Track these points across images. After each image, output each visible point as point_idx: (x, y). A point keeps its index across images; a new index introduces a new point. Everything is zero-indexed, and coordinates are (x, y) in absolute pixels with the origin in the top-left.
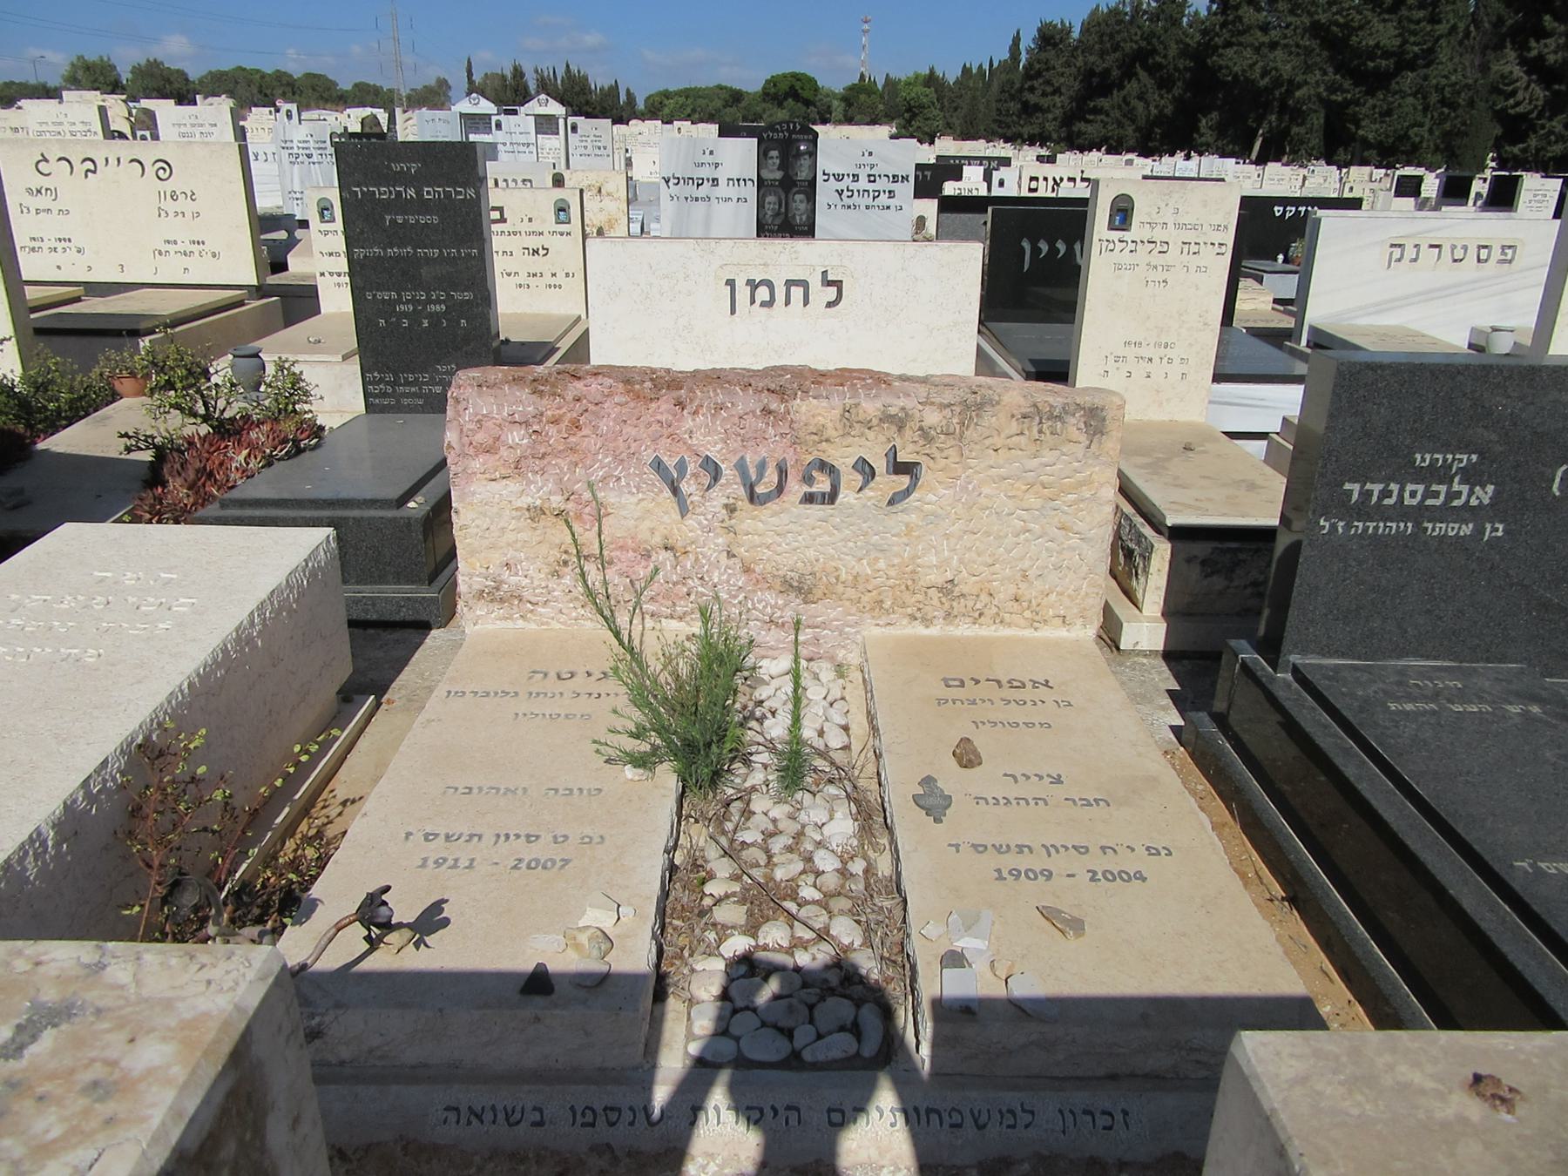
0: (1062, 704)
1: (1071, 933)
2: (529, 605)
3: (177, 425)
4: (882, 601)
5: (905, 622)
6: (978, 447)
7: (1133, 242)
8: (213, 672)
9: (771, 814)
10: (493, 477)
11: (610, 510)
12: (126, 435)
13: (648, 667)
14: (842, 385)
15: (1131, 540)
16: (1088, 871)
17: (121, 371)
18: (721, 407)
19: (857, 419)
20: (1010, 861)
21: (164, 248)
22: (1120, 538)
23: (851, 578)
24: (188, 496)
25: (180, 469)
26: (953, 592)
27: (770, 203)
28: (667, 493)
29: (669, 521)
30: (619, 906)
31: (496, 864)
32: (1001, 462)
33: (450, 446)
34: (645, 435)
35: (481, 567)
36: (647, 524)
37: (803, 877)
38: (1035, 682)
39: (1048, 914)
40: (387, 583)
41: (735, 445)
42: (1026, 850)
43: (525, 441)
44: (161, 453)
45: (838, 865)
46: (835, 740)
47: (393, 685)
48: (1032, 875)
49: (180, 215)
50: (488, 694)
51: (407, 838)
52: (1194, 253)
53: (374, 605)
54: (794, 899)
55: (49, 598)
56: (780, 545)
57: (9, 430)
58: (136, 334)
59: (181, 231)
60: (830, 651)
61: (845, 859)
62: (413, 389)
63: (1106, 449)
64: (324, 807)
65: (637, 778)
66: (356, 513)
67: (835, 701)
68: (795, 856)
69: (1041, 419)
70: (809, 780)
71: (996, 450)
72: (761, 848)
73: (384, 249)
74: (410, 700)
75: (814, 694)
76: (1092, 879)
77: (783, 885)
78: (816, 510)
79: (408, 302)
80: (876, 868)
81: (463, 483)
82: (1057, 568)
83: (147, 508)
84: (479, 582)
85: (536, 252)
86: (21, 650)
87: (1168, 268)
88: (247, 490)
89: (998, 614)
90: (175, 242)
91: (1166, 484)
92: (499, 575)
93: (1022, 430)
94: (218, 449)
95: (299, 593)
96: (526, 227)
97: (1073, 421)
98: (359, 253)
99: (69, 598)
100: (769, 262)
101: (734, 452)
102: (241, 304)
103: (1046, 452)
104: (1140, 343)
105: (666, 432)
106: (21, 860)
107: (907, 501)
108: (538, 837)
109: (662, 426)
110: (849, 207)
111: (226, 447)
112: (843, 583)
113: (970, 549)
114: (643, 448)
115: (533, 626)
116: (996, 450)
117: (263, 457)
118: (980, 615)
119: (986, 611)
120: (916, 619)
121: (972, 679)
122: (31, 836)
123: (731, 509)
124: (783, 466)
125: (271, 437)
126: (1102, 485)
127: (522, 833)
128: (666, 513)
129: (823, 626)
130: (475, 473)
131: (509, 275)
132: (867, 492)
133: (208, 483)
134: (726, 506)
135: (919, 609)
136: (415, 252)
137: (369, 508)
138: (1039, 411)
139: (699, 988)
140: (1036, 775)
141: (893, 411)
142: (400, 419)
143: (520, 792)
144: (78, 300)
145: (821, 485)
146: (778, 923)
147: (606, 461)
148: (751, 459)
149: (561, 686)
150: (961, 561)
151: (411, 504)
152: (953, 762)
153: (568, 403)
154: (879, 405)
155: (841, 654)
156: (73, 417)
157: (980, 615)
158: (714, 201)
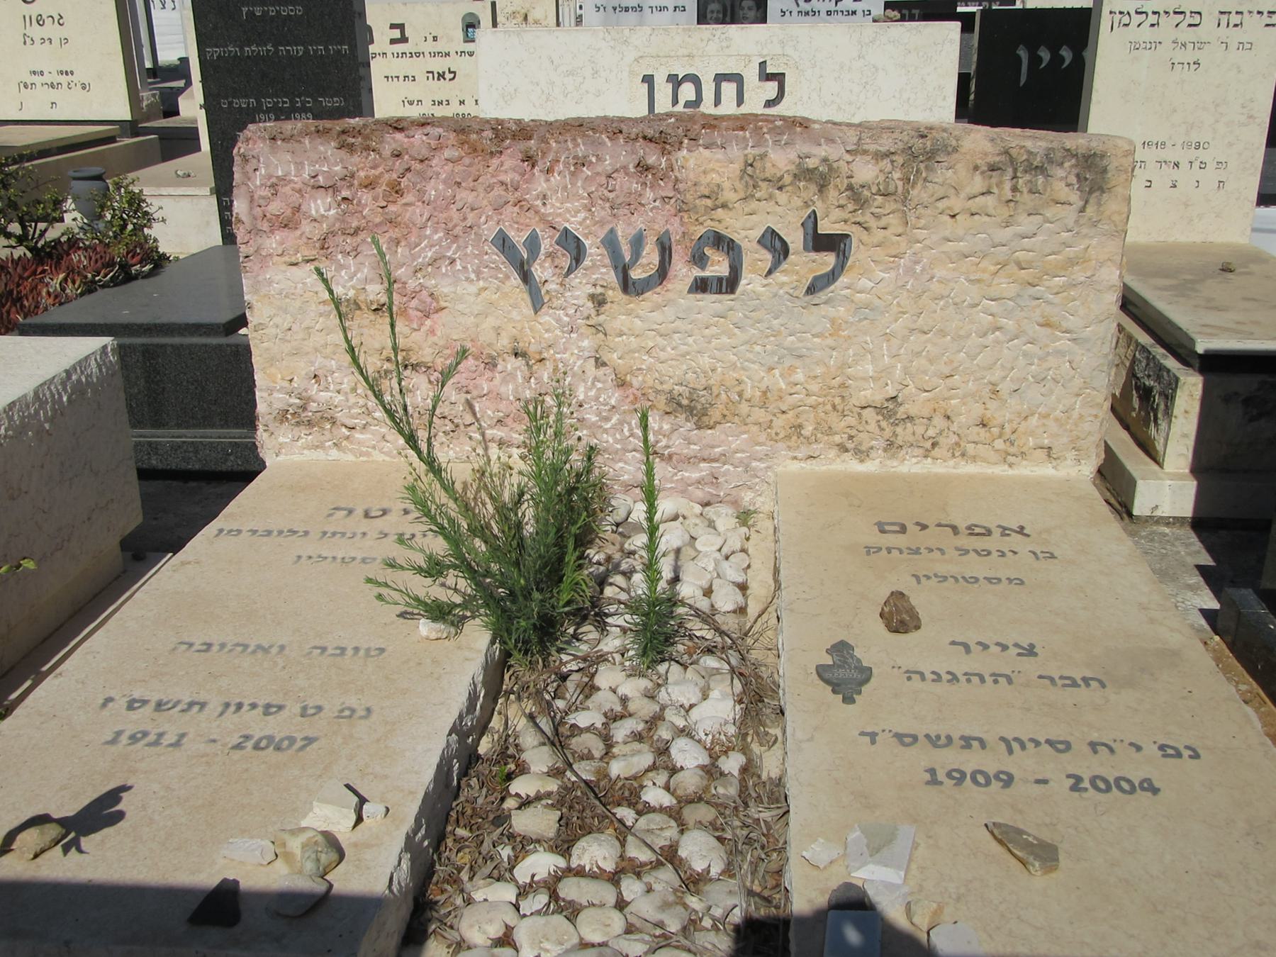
0: (1041, 555)
1: (1037, 864)
2: (344, 430)
4: (800, 426)
5: (832, 453)
6: (929, 211)
7: (1154, 13)
9: (621, 691)
10: (293, 260)
11: (443, 304)
13: (453, 483)
14: (742, 129)
15: (1149, 376)
16: (1069, 776)
18: (581, 163)
19: (762, 176)
20: (950, 758)
21: (30, 79)
22: (1134, 375)
23: (758, 394)
26: (895, 413)
27: (712, 12)
28: (515, 280)
29: (519, 318)
30: (363, 801)
31: (214, 741)
32: (961, 232)
33: (239, 221)
34: (485, 202)
35: (283, 379)
36: (490, 322)
37: (650, 774)
38: (1005, 529)
39: (1004, 836)
40: (213, 426)
41: (603, 213)
42: (975, 744)
43: (333, 212)
45: (704, 759)
46: (726, 600)
48: (981, 778)
49: (47, 42)
50: (269, 533)
51: (104, 705)
52: (1236, 25)
53: (196, 452)
54: (631, 805)
56: (663, 350)
59: (47, 60)
60: (734, 492)
61: (715, 752)
63: (1107, 213)
65: (433, 636)
66: (177, 340)
67: (733, 553)
68: (644, 747)
69: (1015, 170)
70: (680, 648)
71: (953, 216)
72: (600, 735)
73: (242, 49)
75: (704, 545)
76: (1075, 788)
77: (620, 784)
78: (710, 302)
80: (760, 768)
82: (1040, 380)
85: (441, 76)
87: (1199, 45)
89: (957, 444)
90: (42, 73)
91: (1196, 306)
92: (306, 390)
93: (990, 187)
94: (34, 273)
95: (53, 409)
96: (429, 47)
97: (1060, 173)
98: (214, 52)
100: (695, 52)
101: (602, 223)
102: (111, 139)
103: (1023, 218)
104: (1163, 144)
105: (511, 197)
107: (832, 287)
108: (280, 708)
109: (507, 190)
110: (807, 13)
112: (749, 401)
113: (918, 354)
114: (483, 219)
115: (350, 457)
116: (953, 216)
118: (934, 445)
119: (941, 440)
120: (847, 451)
121: (918, 524)
123: (599, 301)
124: (665, 240)
126: (1102, 264)
127: (261, 702)
128: (515, 306)
129: (723, 458)
131: (411, 103)
132: (779, 277)
133: (13, 309)
134: (592, 297)
135: (851, 437)
136: (277, 51)
137: (192, 334)
138: (1012, 160)
139: (471, 926)
140: (998, 644)
141: (811, 163)
143: (274, 650)
145: (717, 268)
146: (603, 837)
147: (436, 237)
148: (624, 233)
149: (365, 525)
150: (906, 371)
152: (880, 626)
153: (385, 160)
154: (793, 155)
155: (747, 497)
157: (934, 445)
158: (647, 11)
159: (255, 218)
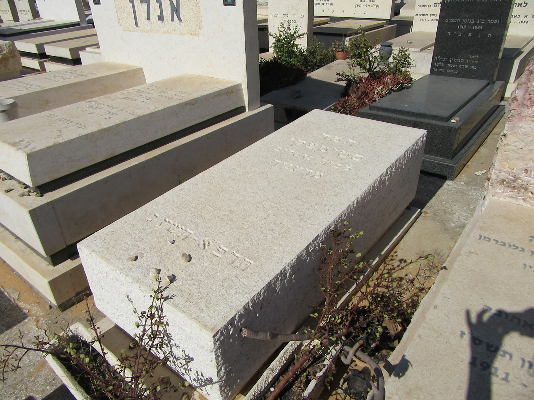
2: (530, 194)
3: (358, 72)
8: (367, 196)
12: (339, 74)
17: (339, 49)
24: (357, 102)
25: (356, 90)
44: (350, 83)
47: (428, 204)
55: (305, 142)
57: (300, 68)
58: (346, 36)
62: (454, 66)
64: (392, 260)
74: (435, 215)
79: (465, 24)
81: (516, 121)
83: (340, 105)
84: (504, 175)
86: (292, 165)
88: (380, 103)
92: (518, 174)
99: (312, 144)
102: (382, 26)
106: (275, 283)
111: (374, 83)
115: (529, 206)
117: (388, 90)
122: (281, 272)
125: (393, 81)
130: (526, 116)
137: (433, 119)
142: (445, 79)
144: (327, 23)
151: (453, 121)
156: (320, 65)
159: (524, 99)
